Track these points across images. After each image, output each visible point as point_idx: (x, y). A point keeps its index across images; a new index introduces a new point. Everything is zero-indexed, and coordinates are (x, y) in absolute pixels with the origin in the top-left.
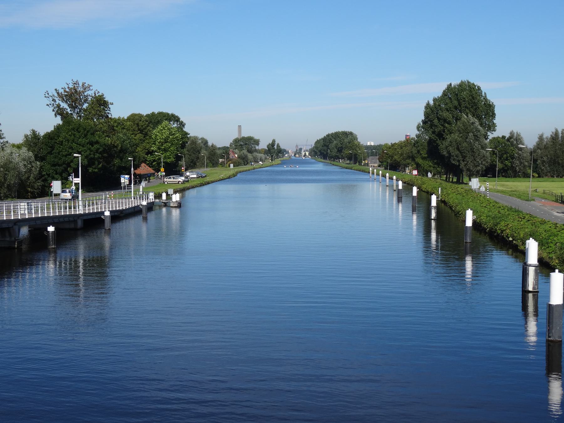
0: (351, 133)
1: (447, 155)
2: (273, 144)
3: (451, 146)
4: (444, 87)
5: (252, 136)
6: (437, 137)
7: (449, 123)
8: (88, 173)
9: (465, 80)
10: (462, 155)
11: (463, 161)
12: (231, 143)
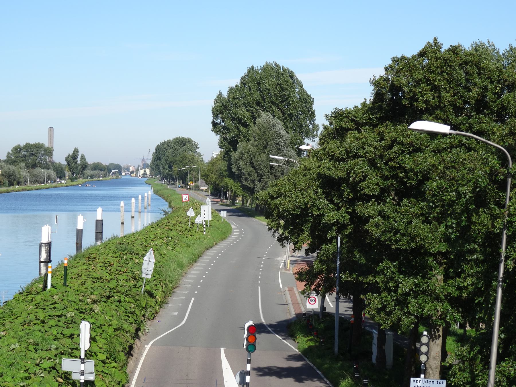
0: (189, 141)
1: (237, 172)
2: (74, 156)
3: (242, 159)
4: (243, 72)
5: (41, 143)
6: (230, 147)
7: (246, 125)
8: (483, 289)
9: (272, 62)
10: (257, 172)
11: (260, 181)
12: (9, 153)
